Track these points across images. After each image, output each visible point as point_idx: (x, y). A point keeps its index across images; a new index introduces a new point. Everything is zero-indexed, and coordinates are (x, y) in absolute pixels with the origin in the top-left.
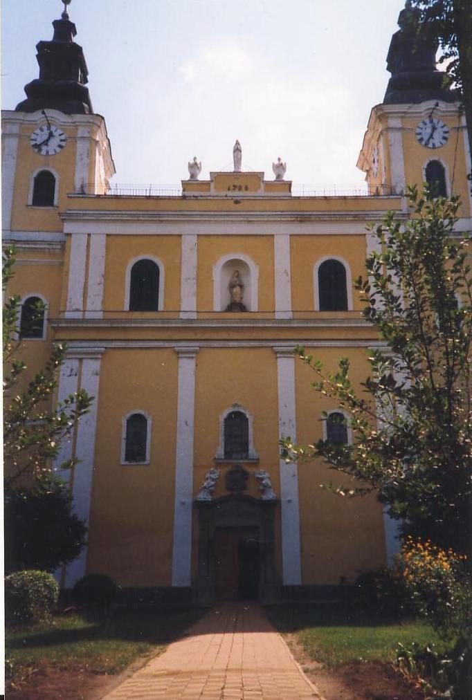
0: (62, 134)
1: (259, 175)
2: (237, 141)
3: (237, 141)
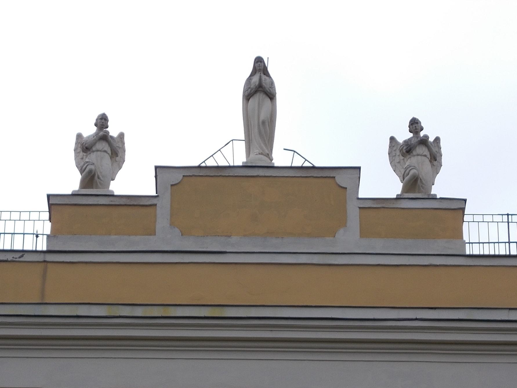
1: (341, 179)
2: (259, 61)
3: (259, 61)
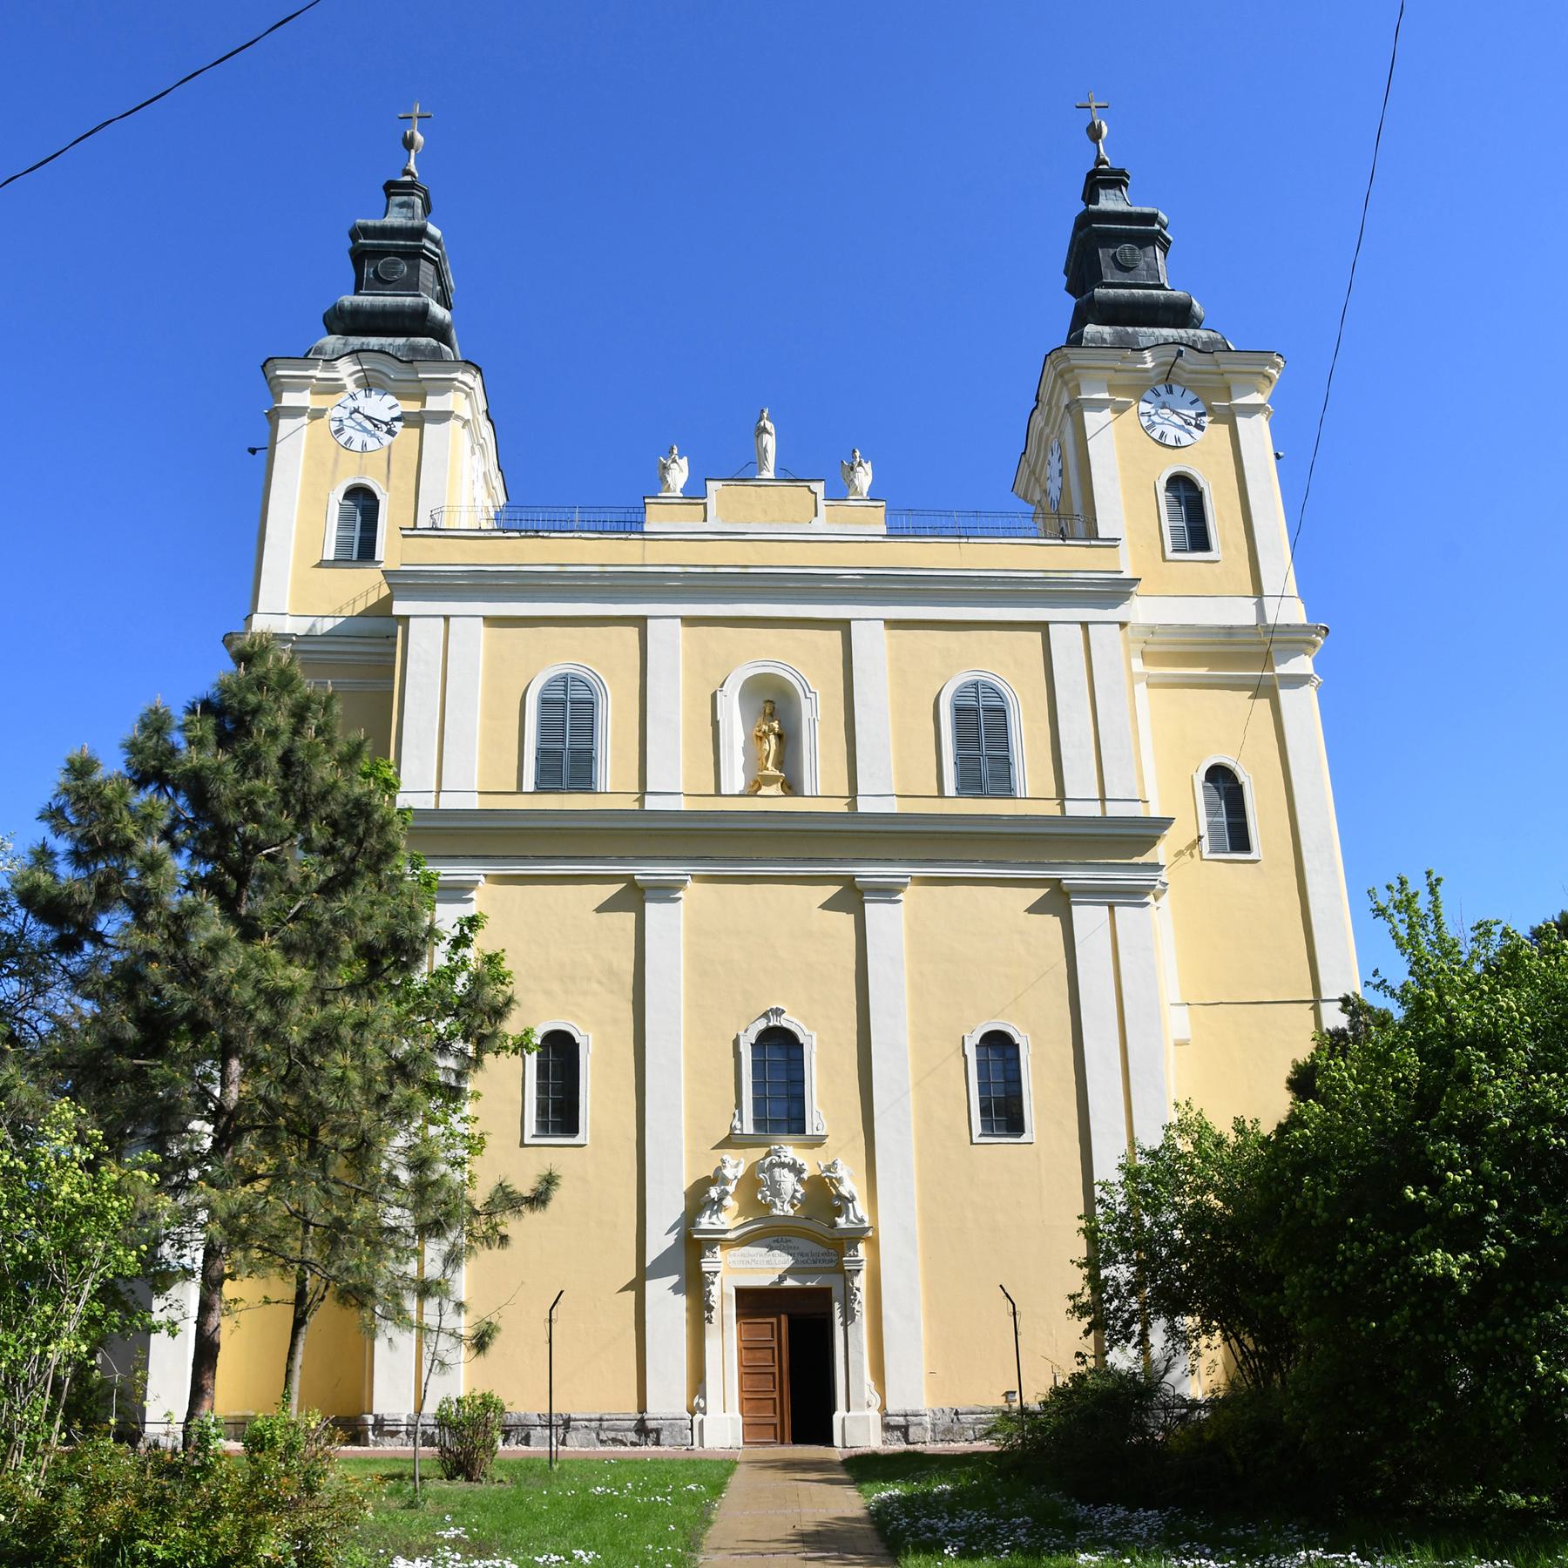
0: (397, 405)
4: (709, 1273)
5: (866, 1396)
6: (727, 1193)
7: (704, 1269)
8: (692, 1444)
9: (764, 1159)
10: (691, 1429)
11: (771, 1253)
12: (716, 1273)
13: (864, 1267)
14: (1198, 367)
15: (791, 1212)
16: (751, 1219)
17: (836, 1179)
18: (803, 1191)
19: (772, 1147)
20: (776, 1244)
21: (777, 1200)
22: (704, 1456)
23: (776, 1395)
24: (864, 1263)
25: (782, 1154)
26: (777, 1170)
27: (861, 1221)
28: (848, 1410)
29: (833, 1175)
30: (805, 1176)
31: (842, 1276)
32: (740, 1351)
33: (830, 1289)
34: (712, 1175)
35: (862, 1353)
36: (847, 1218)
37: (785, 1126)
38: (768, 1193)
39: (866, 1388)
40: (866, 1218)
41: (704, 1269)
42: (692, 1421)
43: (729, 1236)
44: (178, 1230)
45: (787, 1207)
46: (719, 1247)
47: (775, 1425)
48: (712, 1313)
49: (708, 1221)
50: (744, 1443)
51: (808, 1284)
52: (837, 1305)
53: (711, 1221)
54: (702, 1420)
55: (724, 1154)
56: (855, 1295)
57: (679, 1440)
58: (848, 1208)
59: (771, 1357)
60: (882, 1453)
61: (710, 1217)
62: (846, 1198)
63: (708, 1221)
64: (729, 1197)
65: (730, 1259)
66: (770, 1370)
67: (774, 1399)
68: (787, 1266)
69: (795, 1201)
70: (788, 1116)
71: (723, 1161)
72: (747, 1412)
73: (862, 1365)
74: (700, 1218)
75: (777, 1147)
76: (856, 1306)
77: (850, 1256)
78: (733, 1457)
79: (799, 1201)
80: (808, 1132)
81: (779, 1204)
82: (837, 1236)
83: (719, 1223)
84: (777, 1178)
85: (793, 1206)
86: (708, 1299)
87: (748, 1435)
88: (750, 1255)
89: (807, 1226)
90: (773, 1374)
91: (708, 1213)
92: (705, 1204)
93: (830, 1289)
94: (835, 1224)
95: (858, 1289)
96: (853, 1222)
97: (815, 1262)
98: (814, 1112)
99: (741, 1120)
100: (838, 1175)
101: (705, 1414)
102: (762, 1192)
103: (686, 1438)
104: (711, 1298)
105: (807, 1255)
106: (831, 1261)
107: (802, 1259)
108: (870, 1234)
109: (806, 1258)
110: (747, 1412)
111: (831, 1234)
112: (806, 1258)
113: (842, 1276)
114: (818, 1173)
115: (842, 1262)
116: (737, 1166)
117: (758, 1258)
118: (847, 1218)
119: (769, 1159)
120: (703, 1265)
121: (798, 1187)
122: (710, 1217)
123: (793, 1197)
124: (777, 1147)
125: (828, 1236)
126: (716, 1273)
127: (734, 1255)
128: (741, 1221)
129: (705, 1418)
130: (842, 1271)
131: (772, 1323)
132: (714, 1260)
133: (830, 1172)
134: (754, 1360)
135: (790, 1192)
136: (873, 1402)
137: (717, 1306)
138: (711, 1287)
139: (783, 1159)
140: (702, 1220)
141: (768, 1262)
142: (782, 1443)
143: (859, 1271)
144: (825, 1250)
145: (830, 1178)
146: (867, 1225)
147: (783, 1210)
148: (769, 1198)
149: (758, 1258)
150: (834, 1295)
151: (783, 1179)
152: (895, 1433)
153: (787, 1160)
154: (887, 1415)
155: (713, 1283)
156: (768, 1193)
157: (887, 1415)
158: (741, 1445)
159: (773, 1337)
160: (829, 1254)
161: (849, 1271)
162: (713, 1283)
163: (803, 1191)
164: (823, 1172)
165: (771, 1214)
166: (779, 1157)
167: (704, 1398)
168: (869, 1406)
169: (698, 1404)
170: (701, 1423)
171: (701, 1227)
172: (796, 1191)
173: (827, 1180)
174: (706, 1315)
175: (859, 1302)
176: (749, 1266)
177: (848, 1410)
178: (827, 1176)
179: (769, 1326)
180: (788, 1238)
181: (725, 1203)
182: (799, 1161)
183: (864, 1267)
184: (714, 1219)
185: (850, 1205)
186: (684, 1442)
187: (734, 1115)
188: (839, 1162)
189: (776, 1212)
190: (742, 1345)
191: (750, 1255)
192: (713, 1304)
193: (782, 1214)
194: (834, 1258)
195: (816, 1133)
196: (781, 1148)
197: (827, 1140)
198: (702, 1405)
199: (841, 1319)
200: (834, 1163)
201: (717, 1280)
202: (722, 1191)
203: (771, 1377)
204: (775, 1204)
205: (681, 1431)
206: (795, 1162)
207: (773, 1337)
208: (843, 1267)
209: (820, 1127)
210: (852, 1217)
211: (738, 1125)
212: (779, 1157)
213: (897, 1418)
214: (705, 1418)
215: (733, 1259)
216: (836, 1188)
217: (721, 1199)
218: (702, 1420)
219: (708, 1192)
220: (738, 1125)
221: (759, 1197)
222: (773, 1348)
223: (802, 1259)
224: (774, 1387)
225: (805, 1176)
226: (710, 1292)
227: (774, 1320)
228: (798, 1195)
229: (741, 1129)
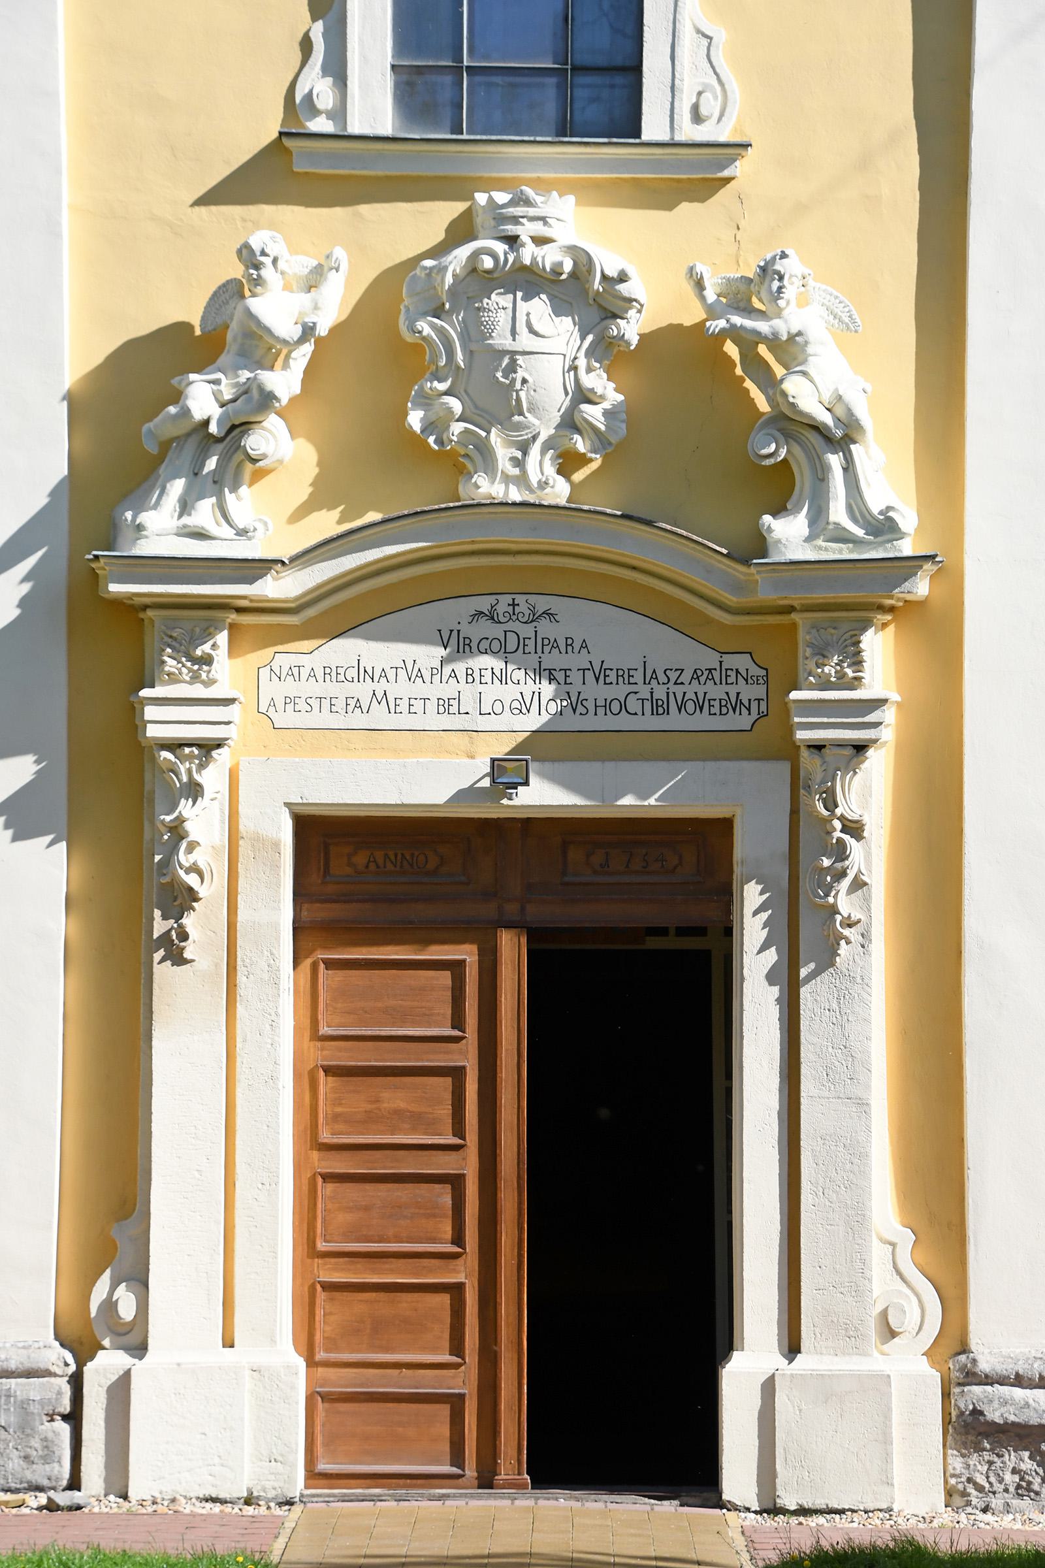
4: (175, 746)
5: (877, 1288)
6: (267, 400)
7: (152, 731)
8: (74, 1484)
9: (439, 251)
10: (74, 1418)
11: (460, 667)
12: (208, 748)
13: (887, 734)
14: (223, 565)
15: (559, 491)
16: (373, 516)
17: (773, 342)
18: (613, 396)
19: (481, 198)
20: (486, 628)
21: (496, 438)
22: (137, 1542)
23: (465, 1273)
24: (888, 715)
25: (525, 231)
26: (499, 300)
27: (884, 527)
28: (792, 1348)
29: (763, 327)
30: (631, 329)
31: (785, 768)
32: (306, 1080)
33: (726, 825)
34: (196, 322)
35: (863, 1105)
36: (818, 516)
37: (548, 97)
38: (456, 405)
39: (878, 1255)
40: (907, 520)
41: (152, 731)
42: (76, 1381)
43: (272, 588)
44: (239, 227)
45: (541, 466)
46: (222, 638)
47: (456, 1402)
48: (188, 921)
49: (174, 523)
50: (314, 1476)
51: (628, 800)
52: (752, 895)
53: (191, 520)
54: (126, 1378)
55: (257, 226)
56: (841, 852)
57: (15, 1464)
58: (821, 475)
59: (445, 1111)
60: (944, 1547)
61: (185, 507)
62: (817, 428)
63: (174, 523)
64: (273, 422)
65: (272, 689)
66: (444, 1164)
67: (456, 1290)
68: (534, 721)
69: (580, 444)
70: (562, 55)
71: (250, 258)
72: (332, 1344)
73: (864, 1156)
74: (139, 509)
75: (501, 197)
76: (845, 902)
77: (826, 685)
78: (253, 1544)
79: (600, 440)
80: (653, 127)
81: (503, 453)
82: (766, 594)
83: (226, 531)
84: (501, 339)
85: (568, 463)
86: (167, 863)
87: (332, 1440)
88: (365, 674)
89: (628, 553)
90: (456, 1182)
91: (177, 487)
92: (165, 447)
93: (726, 825)
94: (760, 545)
95: (854, 829)
96: (842, 537)
97: (659, 708)
98: (687, 37)
99: (337, 69)
100: (782, 327)
101: (139, 1349)
102: (426, 401)
103: (49, 1455)
104: (184, 858)
105: (625, 676)
106: (737, 705)
107: (603, 692)
108: (921, 587)
109: (620, 691)
110: (332, 1344)
111: (738, 587)
112: (620, 691)
113: (785, 768)
114: (690, 314)
115: (786, 710)
116: (313, 281)
117: (401, 688)
118: (818, 516)
119: (462, 253)
120: (150, 712)
121: (597, 381)
122: (185, 507)
123: (570, 423)
124: (501, 197)
125: (731, 599)
126: (208, 748)
127: (294, 673)
128: (326, 524)
129: (140, 1368)
130: (788, 751)
131: (456, 968)
132: (198, 691)
133: (749, 311)
134: (370, 1120)
135: (555, 401)
136: (907, 1318)
137: (211, 891)
138: (185, 808)
139: (529, 252)
140: (146, 518)
141: (445, 706)
142: (486, 1481)
143: (860, 748)
144: (710, 659)
145: (748, 341)
146: (906, 548)
147: (522, 480)
148: (457, 428)
149: (401, 688)
150: (743, 847)
151: (525, 341)
152: (1011, 1459)
153: (549, 257)
154: (972, 1377)
155: (194, 791)
156: (456, 405)
157: (972, 1377)
158: (298, 1484)
159: (458, 1021)
160: (726, 675)
161: (818, 747)
162: (194, 791)
163: (613, 396)
164: (712, 312)
165: (466, 493)
166: (512, 241)
167: (140, 1280)
168: (893, 1334)
169: (110, 1305)
170: (121, 1390)
171: (145, 548)
172: (583, 396)
173: (731, 349)
174: (160, 926)
175: (858, 884)
176: (358, 720)
177: (792, 1348)
178: (733, 333)
179: (445, 978)
180: (542, 603)
181: (254, 442)
182: (608, 262)
183: (887, 734)
184: (204, 513)
185: (835, 461)
186: (38, 1474)
187: (306, 45)
188: (791, 267)
189: (487, 487)
190: (318, 1055)
191: (365, 674)
192: (192, 880)
193: (515, 495)
194: (749, 692)
195: (688, 131)
196: (521, 200)
197: (740, 169)
198: (127, 1309)
199: (771, 956)
200: (765, 270)
201: (212, 778)
202: (244, 391)
203: (444, 1196)
204: (485, 453)
205: (25, 1427)
206: (584, 263)
207: (459, 1130)
208: (790, 729)
209: (710, 106)
210: (838, 512)
211: (324, 92)
212: (512, 241)
213: (1018, 1393)
214: (140, 1368)
215: (290, 687)
216: (770, 384)
217: (237, 429)
218: (126, 1378)
219: (177, 396)
220: (324, 92)
221: (415, 419)
222: (457, 1074)
223: (603, 692)
224: (458, 1239)
225: (631, 329)
226: (178, 831)
227: (467, 953)
228: (594, 413)
229: (339, 113)
